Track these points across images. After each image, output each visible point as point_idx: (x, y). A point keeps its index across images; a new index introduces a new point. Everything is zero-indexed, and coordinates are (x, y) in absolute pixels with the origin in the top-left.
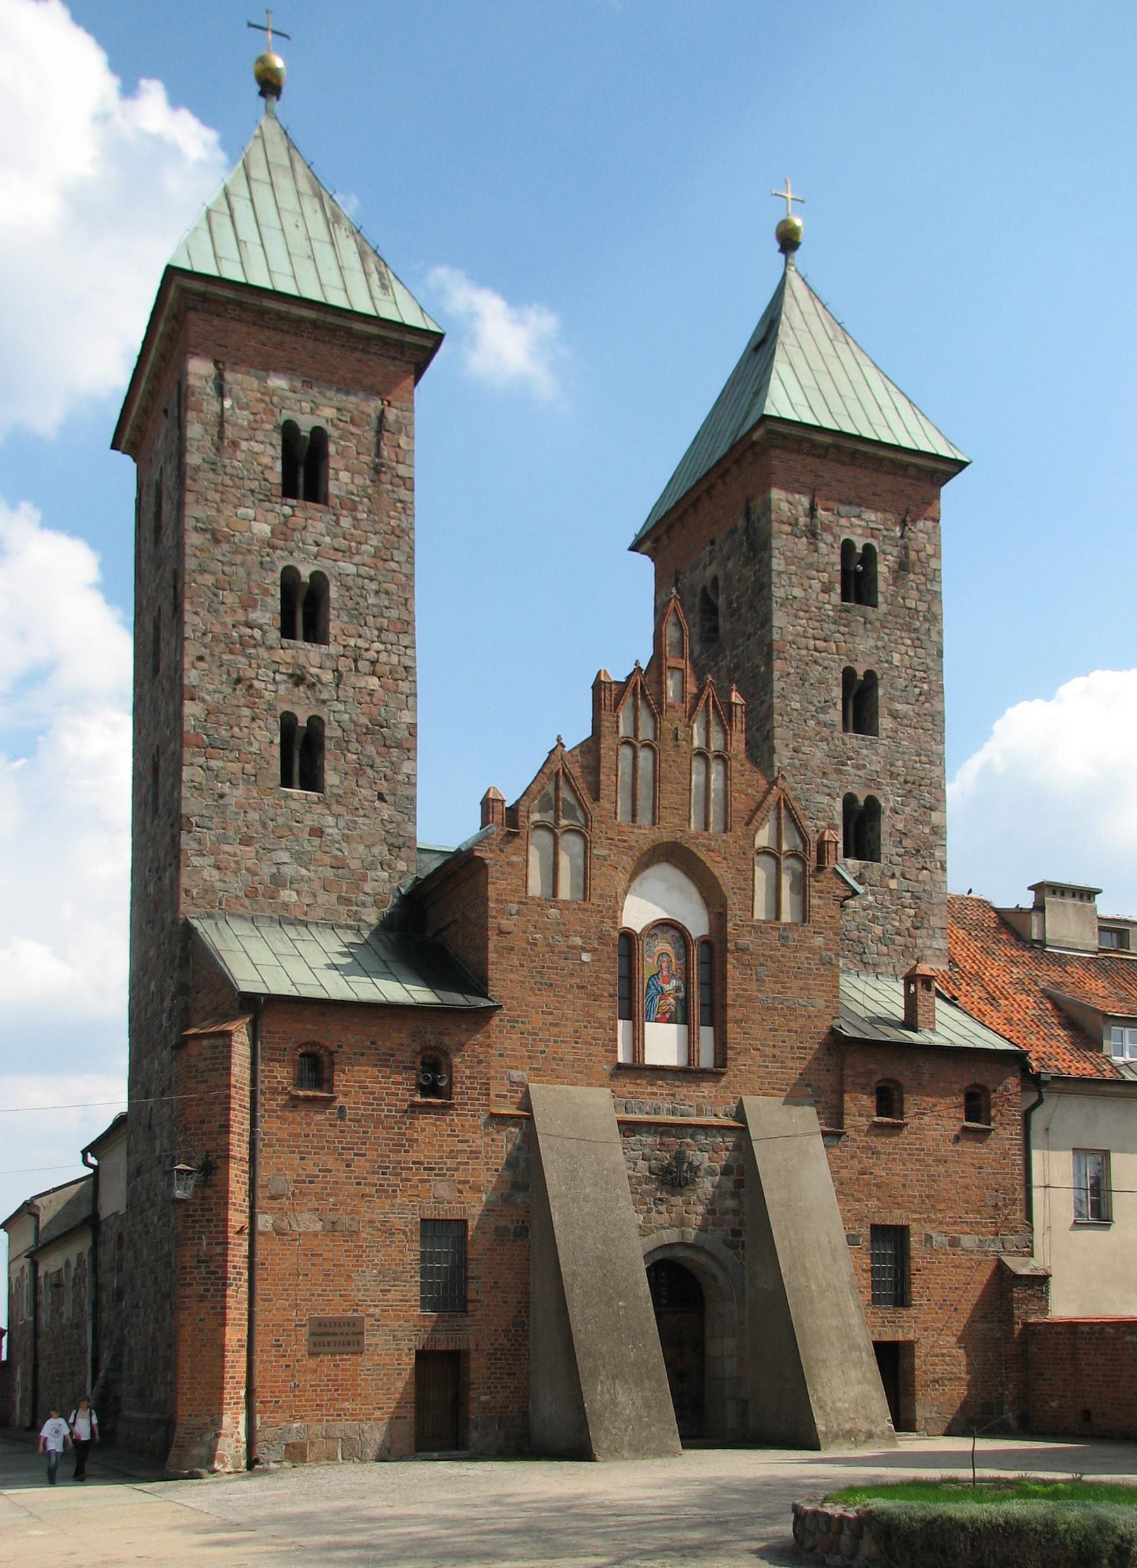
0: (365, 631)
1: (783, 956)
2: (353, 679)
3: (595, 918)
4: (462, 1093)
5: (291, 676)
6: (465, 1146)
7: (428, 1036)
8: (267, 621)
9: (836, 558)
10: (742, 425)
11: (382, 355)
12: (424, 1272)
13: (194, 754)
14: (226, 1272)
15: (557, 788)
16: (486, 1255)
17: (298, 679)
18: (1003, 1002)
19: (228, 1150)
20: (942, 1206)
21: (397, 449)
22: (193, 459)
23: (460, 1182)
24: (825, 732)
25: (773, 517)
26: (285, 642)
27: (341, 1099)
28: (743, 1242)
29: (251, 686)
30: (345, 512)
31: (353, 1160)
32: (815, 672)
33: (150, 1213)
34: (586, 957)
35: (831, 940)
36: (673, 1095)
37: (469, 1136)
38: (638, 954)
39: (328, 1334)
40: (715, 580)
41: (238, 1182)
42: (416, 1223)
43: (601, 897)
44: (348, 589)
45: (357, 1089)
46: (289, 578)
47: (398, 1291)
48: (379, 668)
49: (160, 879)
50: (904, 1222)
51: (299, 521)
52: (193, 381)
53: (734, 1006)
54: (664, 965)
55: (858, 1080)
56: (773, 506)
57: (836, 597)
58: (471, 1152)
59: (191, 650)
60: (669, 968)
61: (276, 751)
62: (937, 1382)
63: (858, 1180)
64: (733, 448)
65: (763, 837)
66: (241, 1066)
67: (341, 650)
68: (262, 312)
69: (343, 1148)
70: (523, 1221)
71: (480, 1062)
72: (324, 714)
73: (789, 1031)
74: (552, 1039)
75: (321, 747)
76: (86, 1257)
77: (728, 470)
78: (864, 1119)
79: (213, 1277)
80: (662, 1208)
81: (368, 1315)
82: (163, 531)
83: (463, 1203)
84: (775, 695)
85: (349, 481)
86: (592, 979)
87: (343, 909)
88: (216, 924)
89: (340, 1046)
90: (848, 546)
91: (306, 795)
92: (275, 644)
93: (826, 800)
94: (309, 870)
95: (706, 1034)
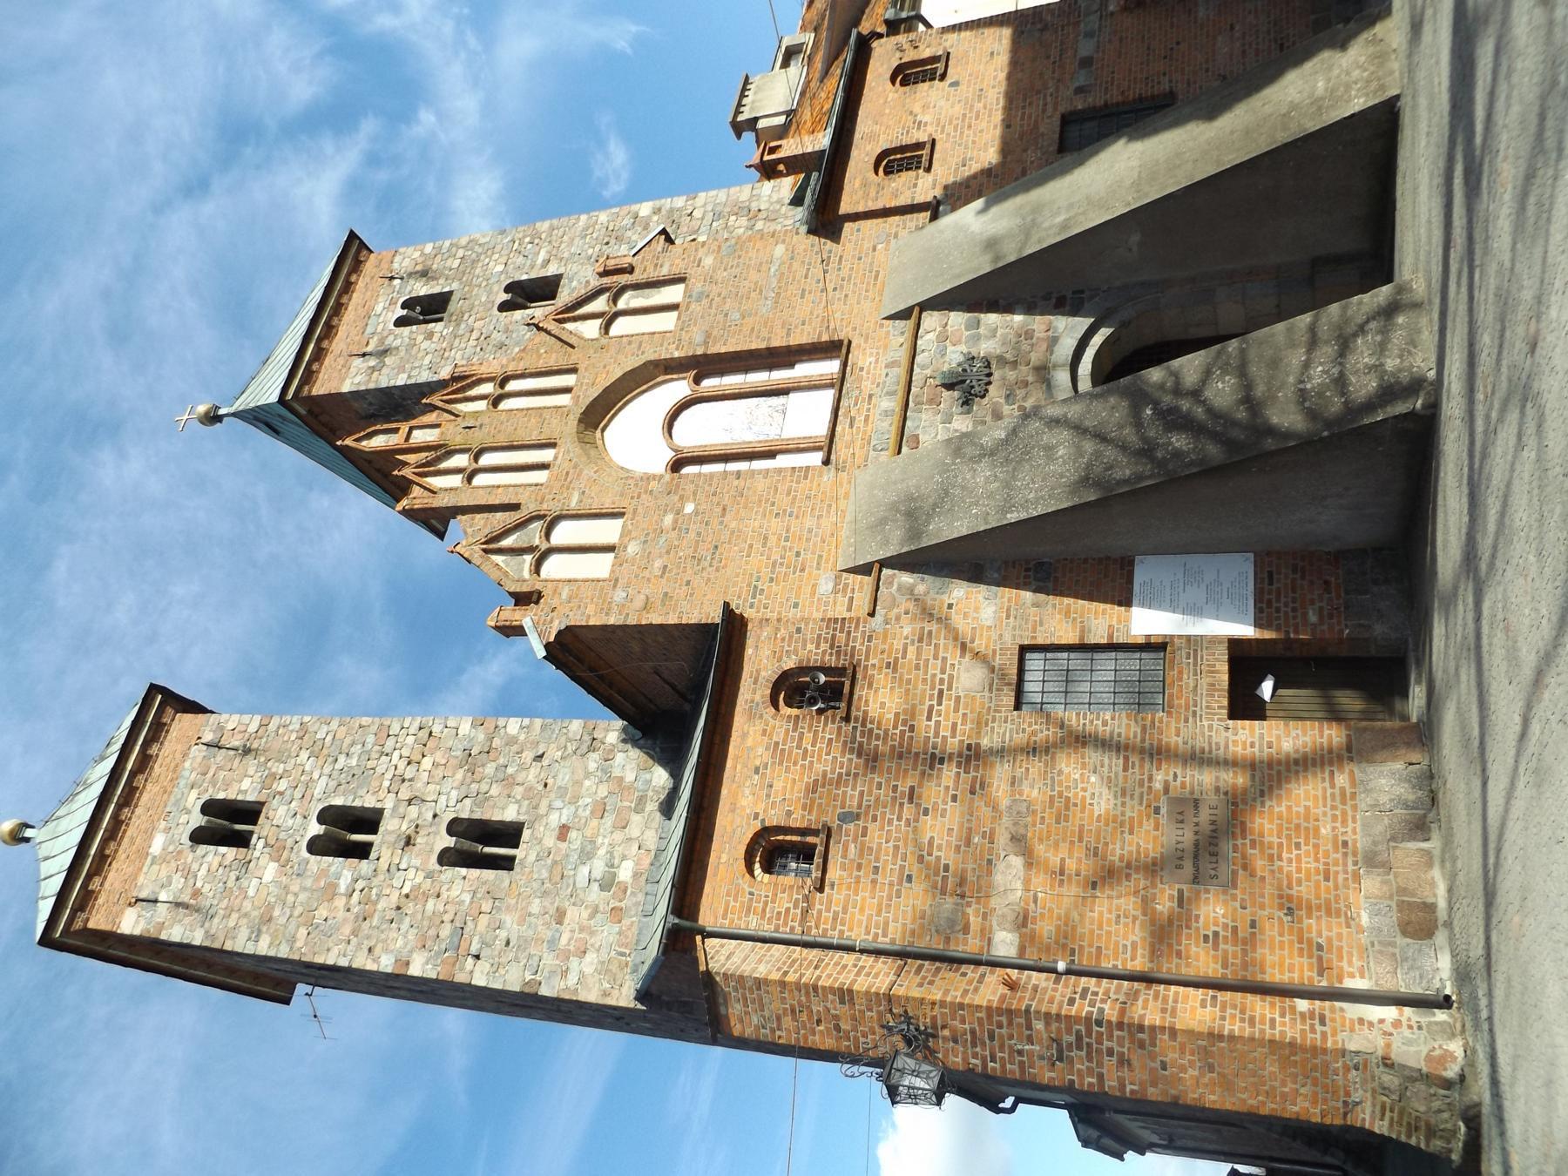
0: (379, 770)
1: (719, 295)
2: (419, 785)
6: (911, 650)
9: (406, 331)
13: (462, 969)
14: (1078, 1019)
16: (1075, 619)
26: (373, 855)
28: (1074, 293)
29: (407, 896)
30: (274, 786)
32: (497, 337)
36: (870, 396)
45: (817, 795)
46: (316, 846)
48: (415, 758)
61: (474, 873)
70: (1027, 570)
71: (799, 630)
73: (806, 277)
74: (783, 543)
79: (1086, 1040)
90: (400, 322)
94: (603, 844)
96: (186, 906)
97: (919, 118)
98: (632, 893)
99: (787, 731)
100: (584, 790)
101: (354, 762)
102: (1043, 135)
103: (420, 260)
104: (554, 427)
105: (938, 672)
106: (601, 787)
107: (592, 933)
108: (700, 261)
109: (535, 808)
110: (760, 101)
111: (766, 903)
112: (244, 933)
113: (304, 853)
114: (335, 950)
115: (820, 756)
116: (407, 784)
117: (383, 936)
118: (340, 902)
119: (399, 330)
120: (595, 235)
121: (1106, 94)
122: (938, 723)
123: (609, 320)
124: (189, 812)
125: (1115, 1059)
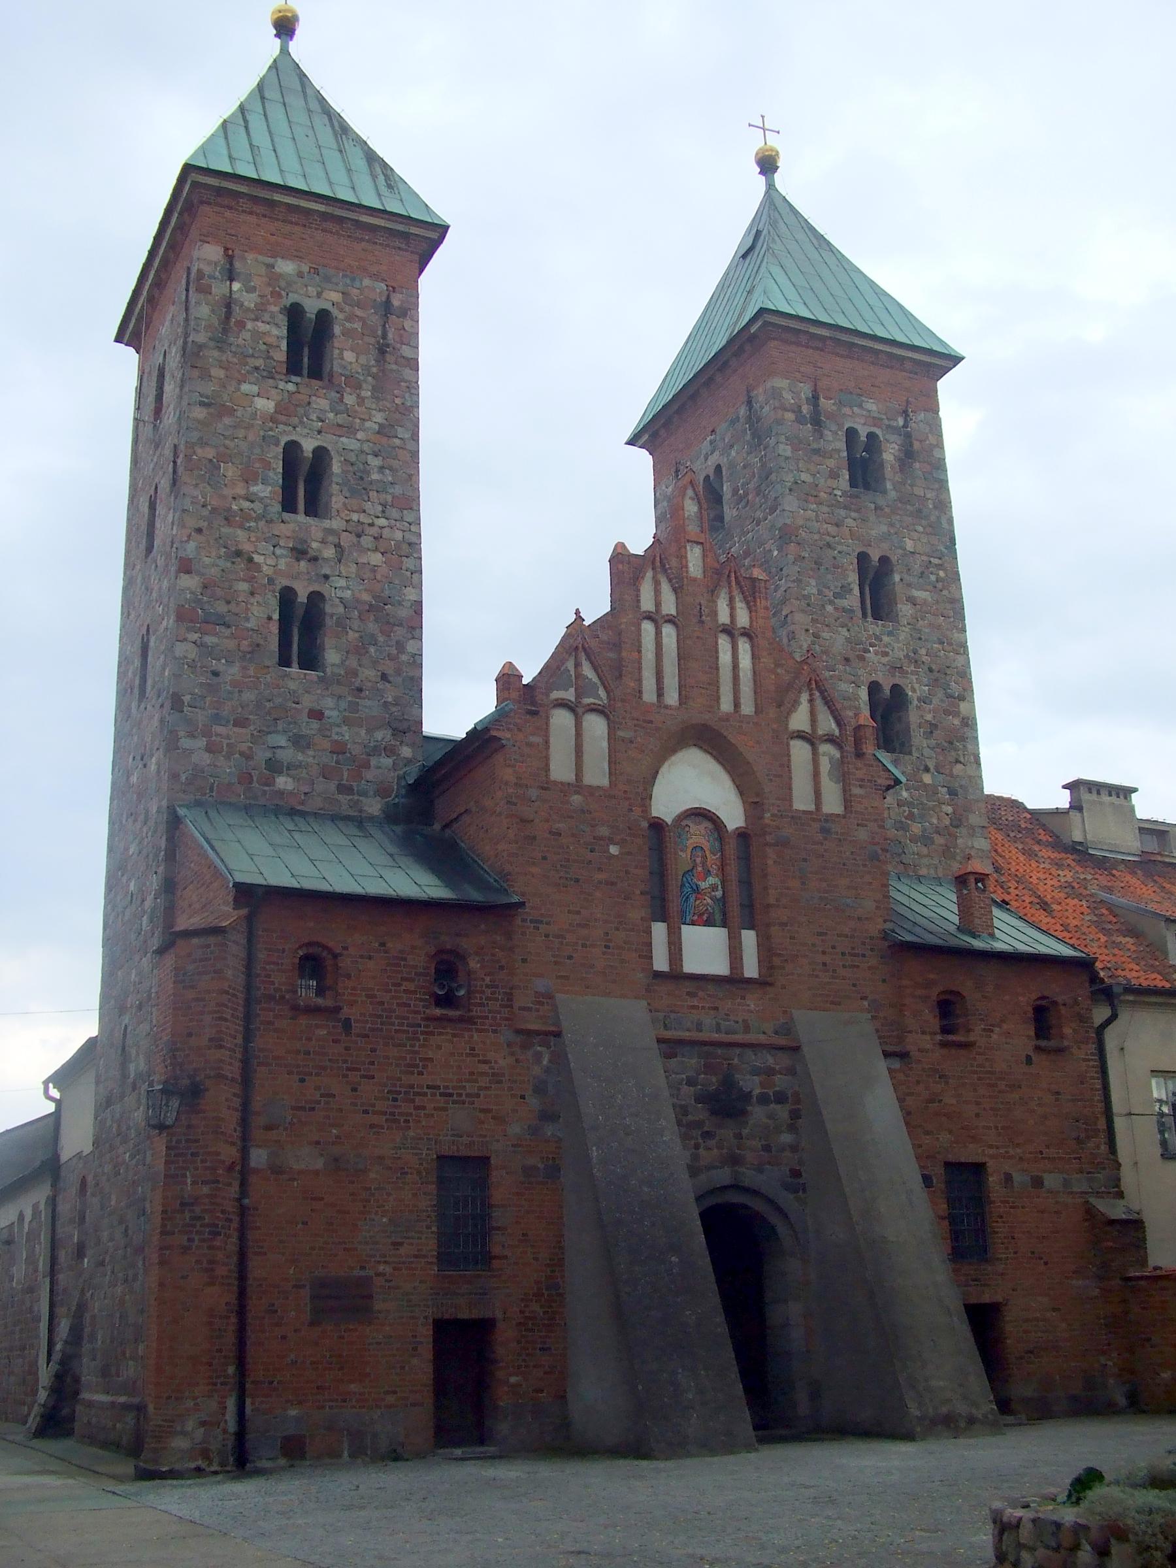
0: (368, 506)
4: (481, 1005)
5: (292, 549)
6: (484, 1068)
8: (268, 495)
9: (841, 445)
10: (736, 322)
11: (387, 246)
15: (577, 665)
17: (300, 552)
21: (402, 332)
23: (482, 1111)
26: (286, 516)
27: (345, 1009)
29: (251, 560)
33: (121, 1150)
34: (614, 850)
35: (877, 833)
36: (716, 1009)
40: (718, 468)
42: (432, 1160)
45: (364, 999)
47: (412, 1244)
49: (145, 766)
54: (698, 860)
58: (493, 1074)
61: (274, 628)
62: (1031, 1352)
64: (731, 342)
67: (343, 525)
68: (272, 204)
69: (348, 1069)
71: (502, 968)
72: (324, 589)
74: (580, 942)
76: (42, 1207)
78: (928, 1037)
79: (198, 1224)
81: (378, 1275)
82: (163, 411)
83: (485, 1136)
85: (354, 360)
87: (343, 799)
88: (206, 813)
89: (346, 948)
90: (851, 434)
91: (305, 674)
92: (275, 517)
93: (851, 688)
95: (749, 938)
98: (265, 792)
99: (416, 967)
101: (375, 476)
105: (468, 1091)
107: (228, 757)
108: (863, 825)
113: (284, 440)
114: (196, 493)
116: (355, 540)
118: (240, 490)
119: (842, 434)
121: (1001, 1202)
122: (425, 1094)
124: (319, 295)
125: (186, 1243)
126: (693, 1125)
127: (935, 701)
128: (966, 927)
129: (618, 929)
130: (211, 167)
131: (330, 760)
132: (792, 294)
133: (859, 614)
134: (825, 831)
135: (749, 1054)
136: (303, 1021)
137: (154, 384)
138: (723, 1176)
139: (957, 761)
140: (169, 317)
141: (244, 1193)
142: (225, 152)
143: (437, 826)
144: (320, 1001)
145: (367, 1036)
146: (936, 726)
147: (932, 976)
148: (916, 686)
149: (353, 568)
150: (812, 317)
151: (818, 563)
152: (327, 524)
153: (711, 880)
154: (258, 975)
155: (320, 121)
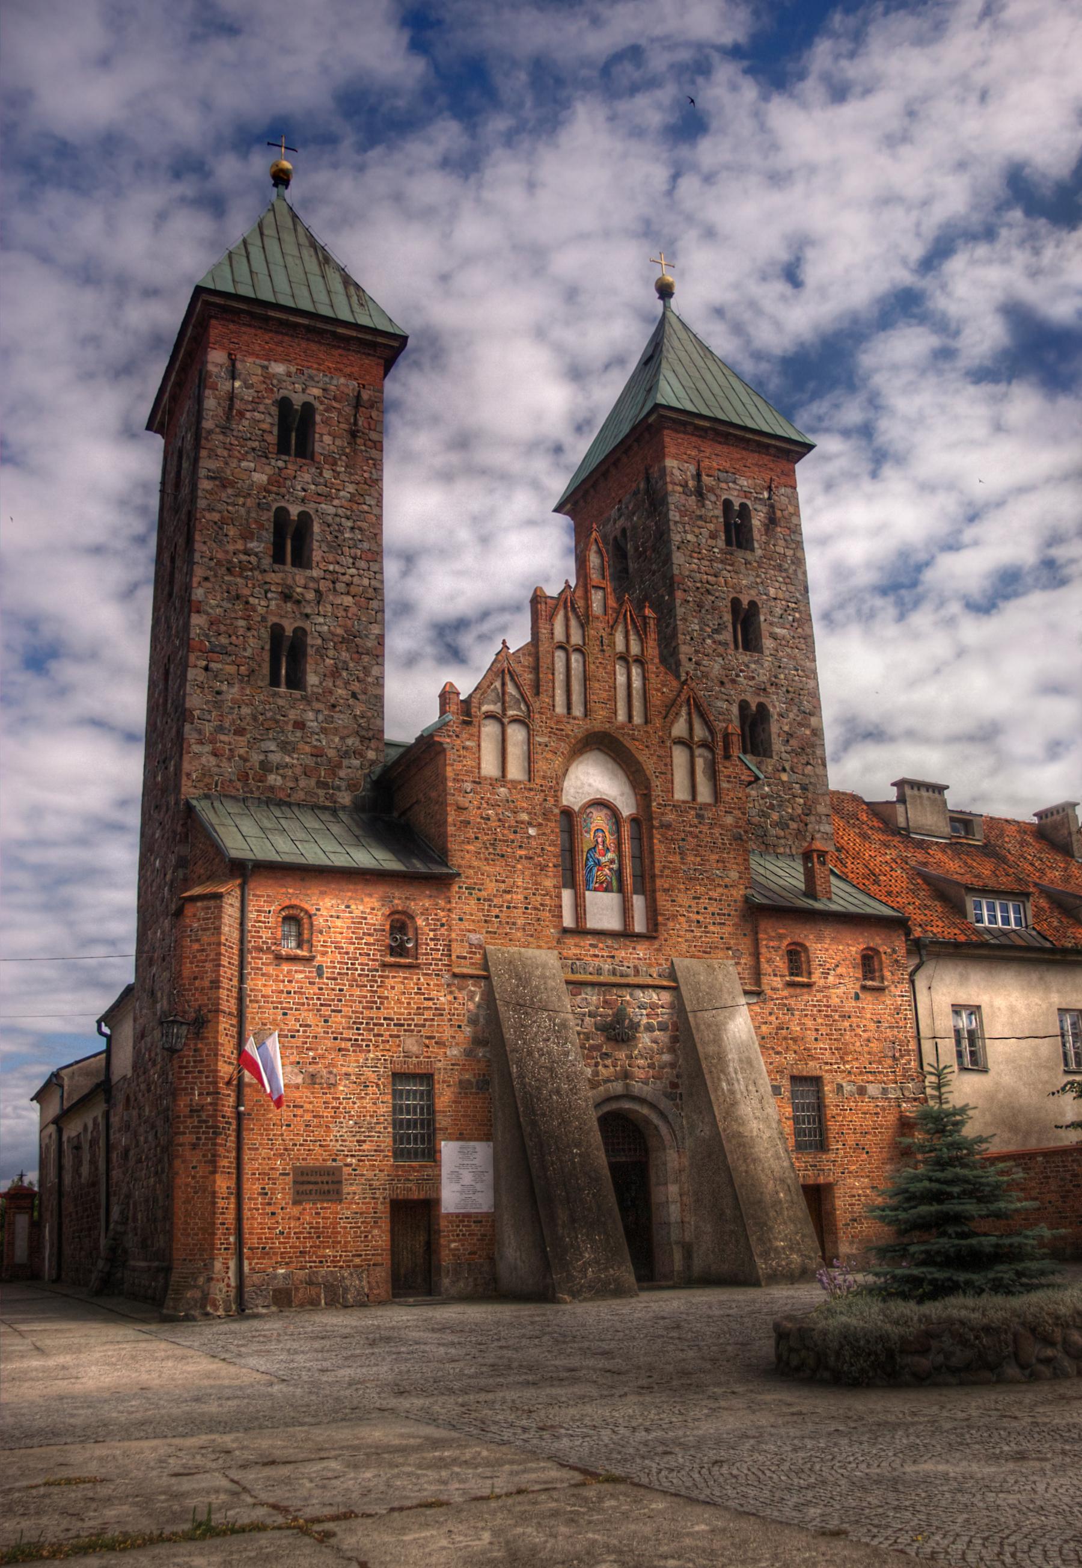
0: (342, 559)
3: (539, 798)
4: (427, 954)
6: (430, 1004)
7: (396, 901)
9: (719, 512)
12: (397, 1124)
13: (198, 658)
15: (503, 684)
17: (286, 597)
18: (882, 878)
19: (218, 1004)
20: (850, 1058)
22: (208, 424)
23: (428, 1038)
24: (721, 649)
25: (668, 480)
26: (276, 567)
27: (319, 958)
28: (681, 1094)
29: (247, 603)
30: (327, 466)
31: (330, 1016)
34: (532, 831)
36: (613, 957)
37: (434, 994)
38: (577, 828)
39: (309, 1183)
40: (624, 531)
41: (227, 1035)
43: (544, 777)
44: (329, 526)
47: (372, 1141)
48: (353, 590)
50: (818, 1073)
51: (290, 472)
52: (210, 367)
53: (662, 876)
54: (600, 840)
55: (772, 944)
56: (668, 471)
57: (721, 543)
58: (436, 1009)
59: (199, 572)
60: (603, 842)
61: (266, 656)
62: (855, 1220)
63: (776, 1034)
64: (634, 429)
65: (679, 729)
66: (230, 926)
67: (322, 574)
68: (267, 319)
69: (321, 1005)
71: (442, 925)
72: (307, 625)
75: (304, 654)
76: (100, 1119)
77: (630, 447)
78: (779, 979)
80: (609, 1062)
81: (347, 1165)
83: (429, 1057)
84: (679, 618)
86: (538, 851)
87: (321, 792)
89: (318, 910)
94: (293, 758)
95: (638, 902)
96: (231, 407)
97: (832, 972)
98: (259, 787)
100: (332, 737)
102: (806, 1064)
103: (786, 513)
104: (601, 714)
106: (335, 751)
107: (229, 759)
109: (318, 700)
110: (921, 804)
111: (264, 922)
112: (213, 464)
113: (275, 506)
114: (205, 548)
115: (359, 949)
116: (331, 586)
117: (217, 587)
119: (720, 504)
120: (797, 678)
122: (382, 1025)
123: (687, 743)
124: (304, 391)
126: (592, 1048)
127: (791, 715)
128: (810, 892)
129: (534, 894)
130: (218, 288)
131: (310, 761)
132: (681, 393)
133: (732, 646)
134: (699, 816)
135: (639, 993)
136: (285, 967)
137: (175, 463)
138: (618, 1087)
139: (808, 763)
140: (186, 409)
141: (239, 1102)
142: (229, 276)
143: (395, 814)
144: (299, 952)
145: (335, 979)
146: (791, 735)
147: (781, 931)
148: (777, 704)
149: (329, 608)
150: (695, 410)
151: (700, 605)
152: (308, 573)
153: (610, 855)
154: (250, 931)
155: (307, 253)
